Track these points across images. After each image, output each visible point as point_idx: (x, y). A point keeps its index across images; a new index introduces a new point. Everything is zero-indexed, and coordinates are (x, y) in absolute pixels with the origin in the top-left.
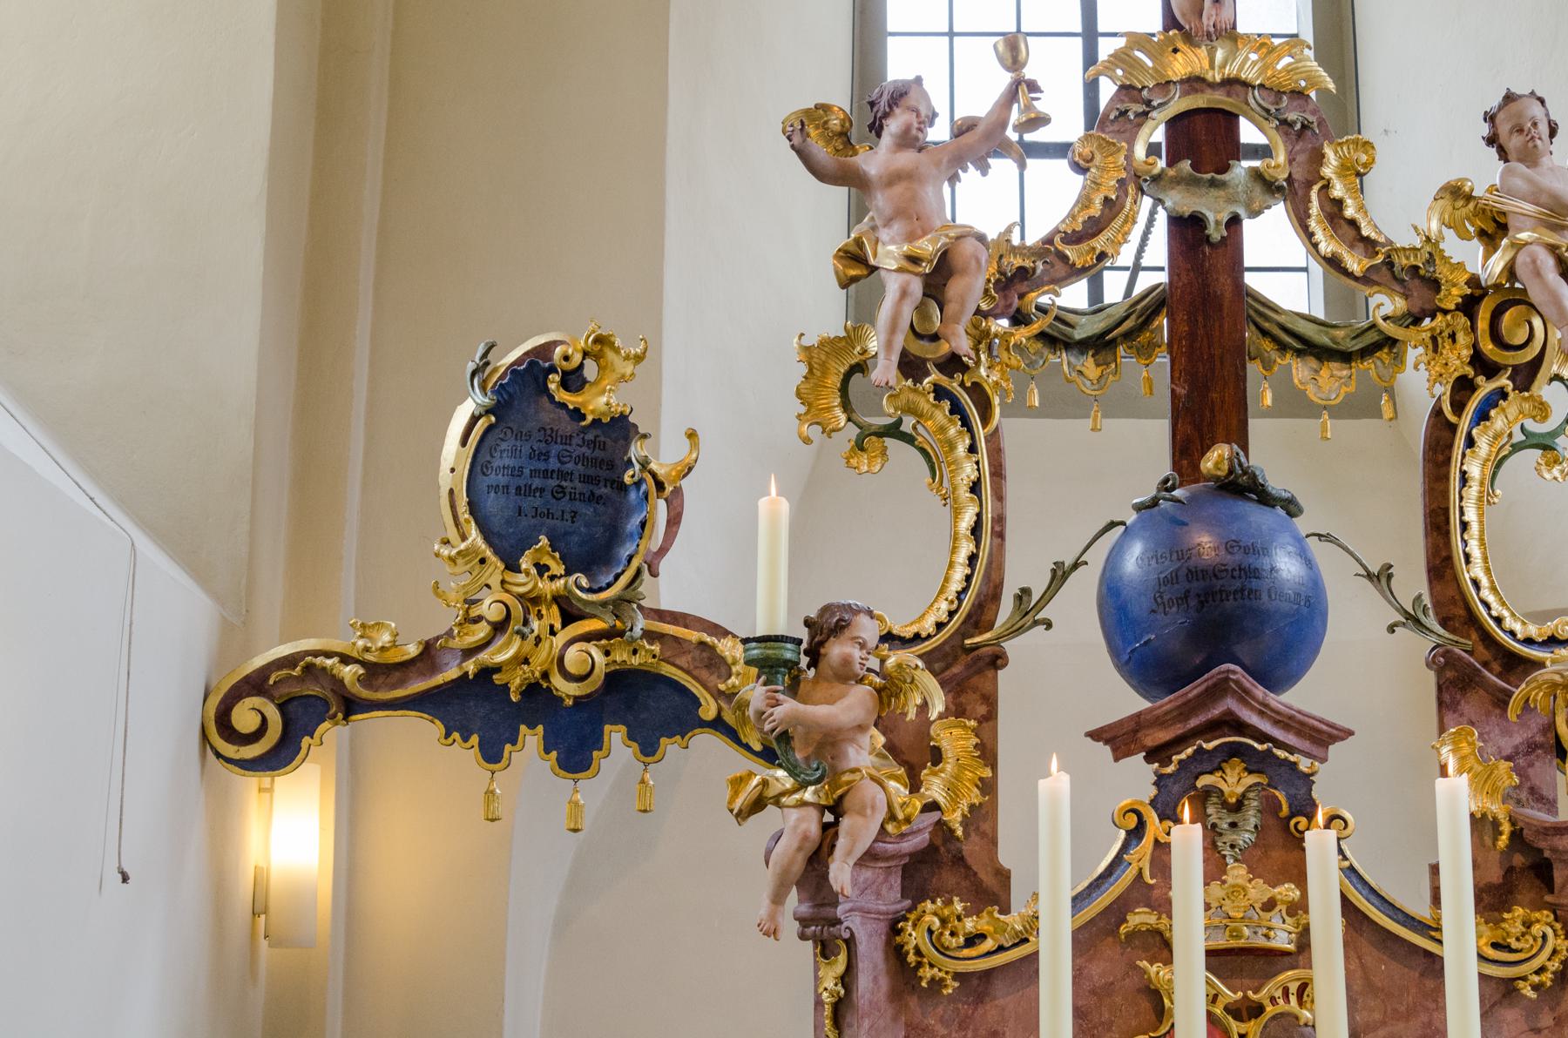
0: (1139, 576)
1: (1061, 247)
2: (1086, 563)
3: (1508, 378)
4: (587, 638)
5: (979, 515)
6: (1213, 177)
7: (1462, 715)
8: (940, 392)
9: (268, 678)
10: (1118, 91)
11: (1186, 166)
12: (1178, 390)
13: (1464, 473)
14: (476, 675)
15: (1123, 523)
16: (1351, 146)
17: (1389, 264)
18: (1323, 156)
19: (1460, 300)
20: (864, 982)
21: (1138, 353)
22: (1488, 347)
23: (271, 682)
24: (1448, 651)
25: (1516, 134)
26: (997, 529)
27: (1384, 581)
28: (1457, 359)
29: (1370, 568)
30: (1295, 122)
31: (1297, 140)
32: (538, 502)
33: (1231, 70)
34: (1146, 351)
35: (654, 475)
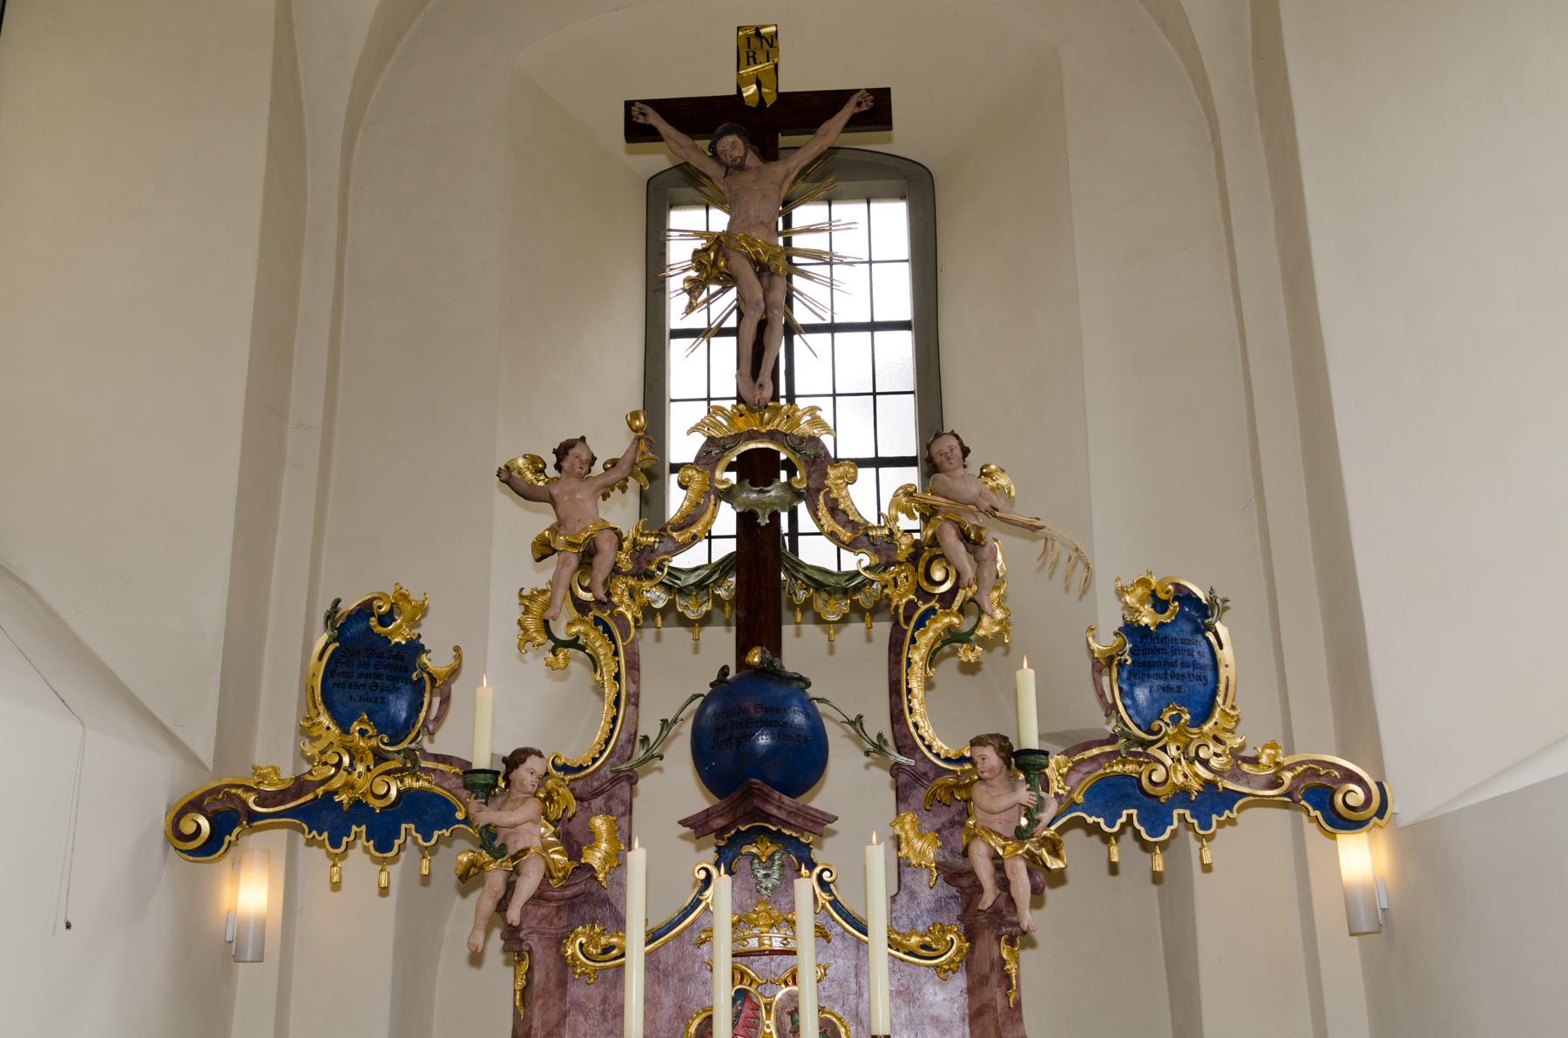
0: (793, 721)
4: (388, 773)
7: (910, 805)
9: (204, 801)
10: (707, 440)
13: (909, 660)
14: (322, 796)
20: (538, 977)
22: (924, 584)
23: (205, 804)
31: (812, 466)
32: (361, 692)
35: (429, 674)
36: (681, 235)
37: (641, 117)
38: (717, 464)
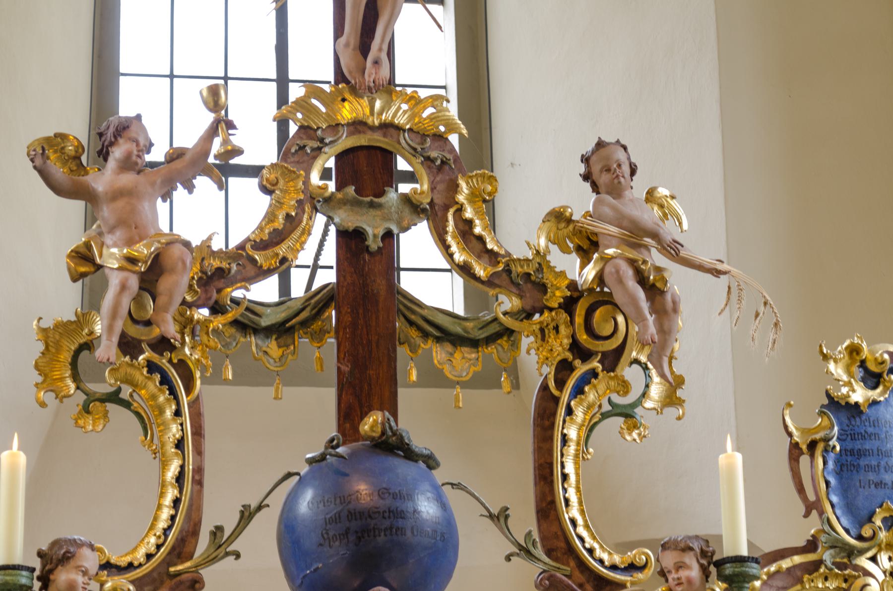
2: (268, 506)
3: (599, 362)
5: (182, 467)
6: (371, 200)
8: (152, 367)
10: (298, 130)
11: (351, 190)
12: (343, 368)
13: (564, 436)
15: (298, 474)
16: (479, 179)
17: (508, 271)
18: (458, 186)
19: (562, 300)
21: (312, 338)
22: (583, 337)
24: (551, 576)
25: (605, 173)
26: (197, 477)
27: (502, 520)
28: (560, 346)
29: (491, 510)
30: (436, 159)
31: (438, 173)
33: (387, 116)
34: (318, 337)
38: (313, 164)
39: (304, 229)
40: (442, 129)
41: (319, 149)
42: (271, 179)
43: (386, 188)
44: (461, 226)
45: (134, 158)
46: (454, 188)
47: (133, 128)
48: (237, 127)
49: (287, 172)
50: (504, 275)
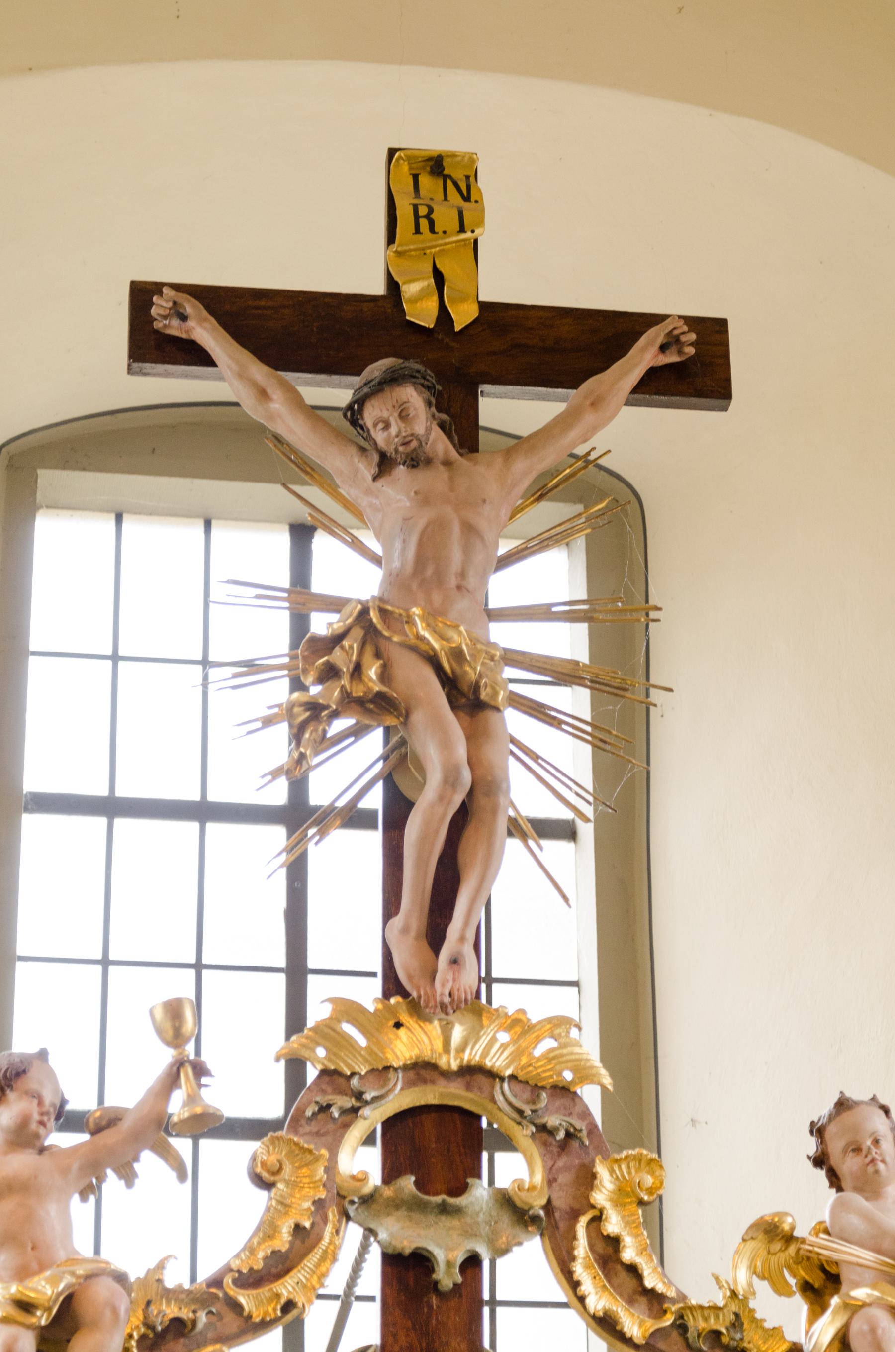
1: (232, 1291)
11: (408, 1183)
16: (632, 1165)
17: (681, 1326)
18: (594, 1176)
25: (851, 1154)
30: (556, 1130)
31: (559, 1155)
33: (473, 1055)
36: (258, 597)
37: (175, 322)
38: (342, 1136)
39: (325, 1252)
40: (568, 1076)
41: (355, 1111)
42: (269, 1163)
43: (469, 1180)
44: (600, 1247)
45: (34, 1126)
46: (588, 1179)
47: (34, 1074)
48: (213, 1074)
49: (297, 1152)
50: (675, 1334)
